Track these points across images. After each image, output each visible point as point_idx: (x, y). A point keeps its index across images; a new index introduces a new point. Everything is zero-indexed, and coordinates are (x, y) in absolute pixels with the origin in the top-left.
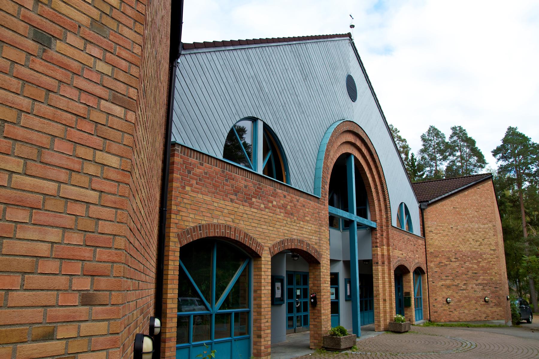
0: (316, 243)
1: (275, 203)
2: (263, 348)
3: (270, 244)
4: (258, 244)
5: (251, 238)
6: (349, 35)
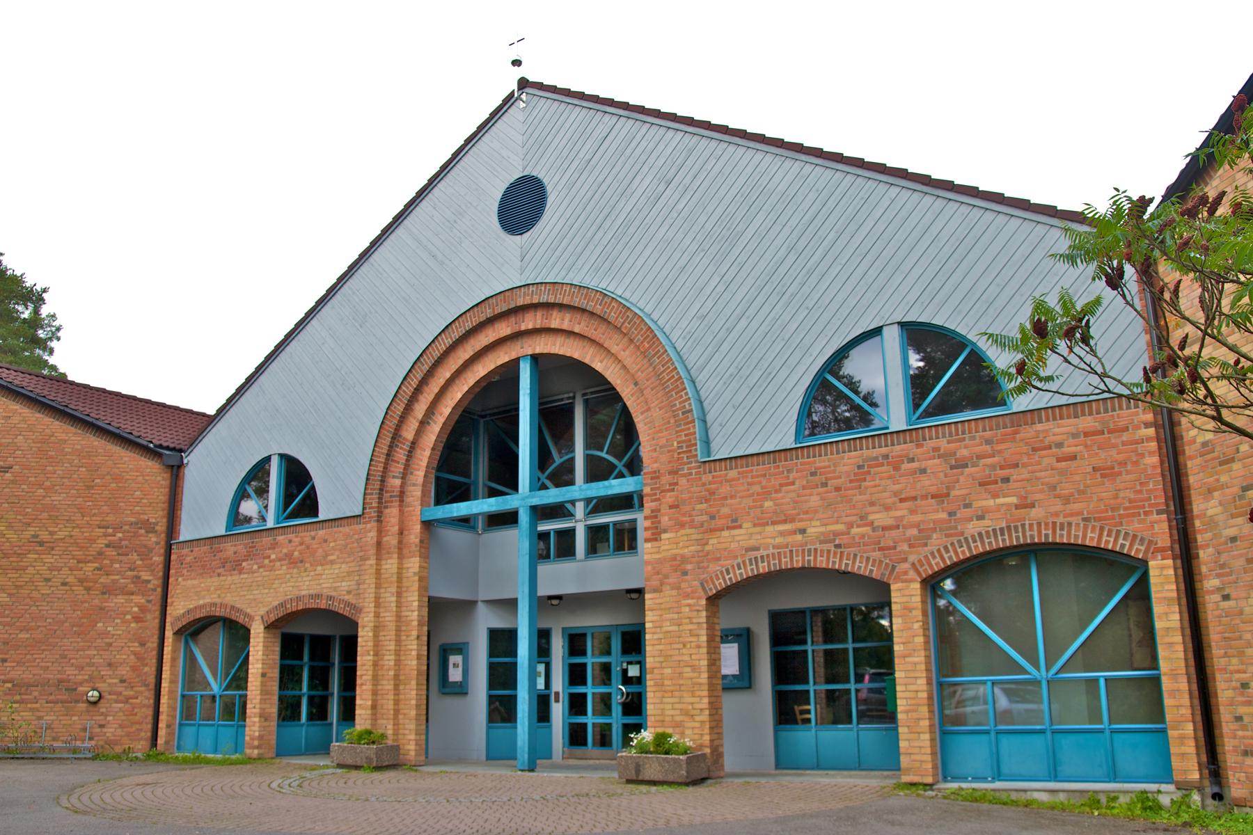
0: (349, 592)
1: (273, 557)
2: (247, 738)
3: (262, 611)
4: (247, 615)
5: (238, 610)
6: (523, 84)
